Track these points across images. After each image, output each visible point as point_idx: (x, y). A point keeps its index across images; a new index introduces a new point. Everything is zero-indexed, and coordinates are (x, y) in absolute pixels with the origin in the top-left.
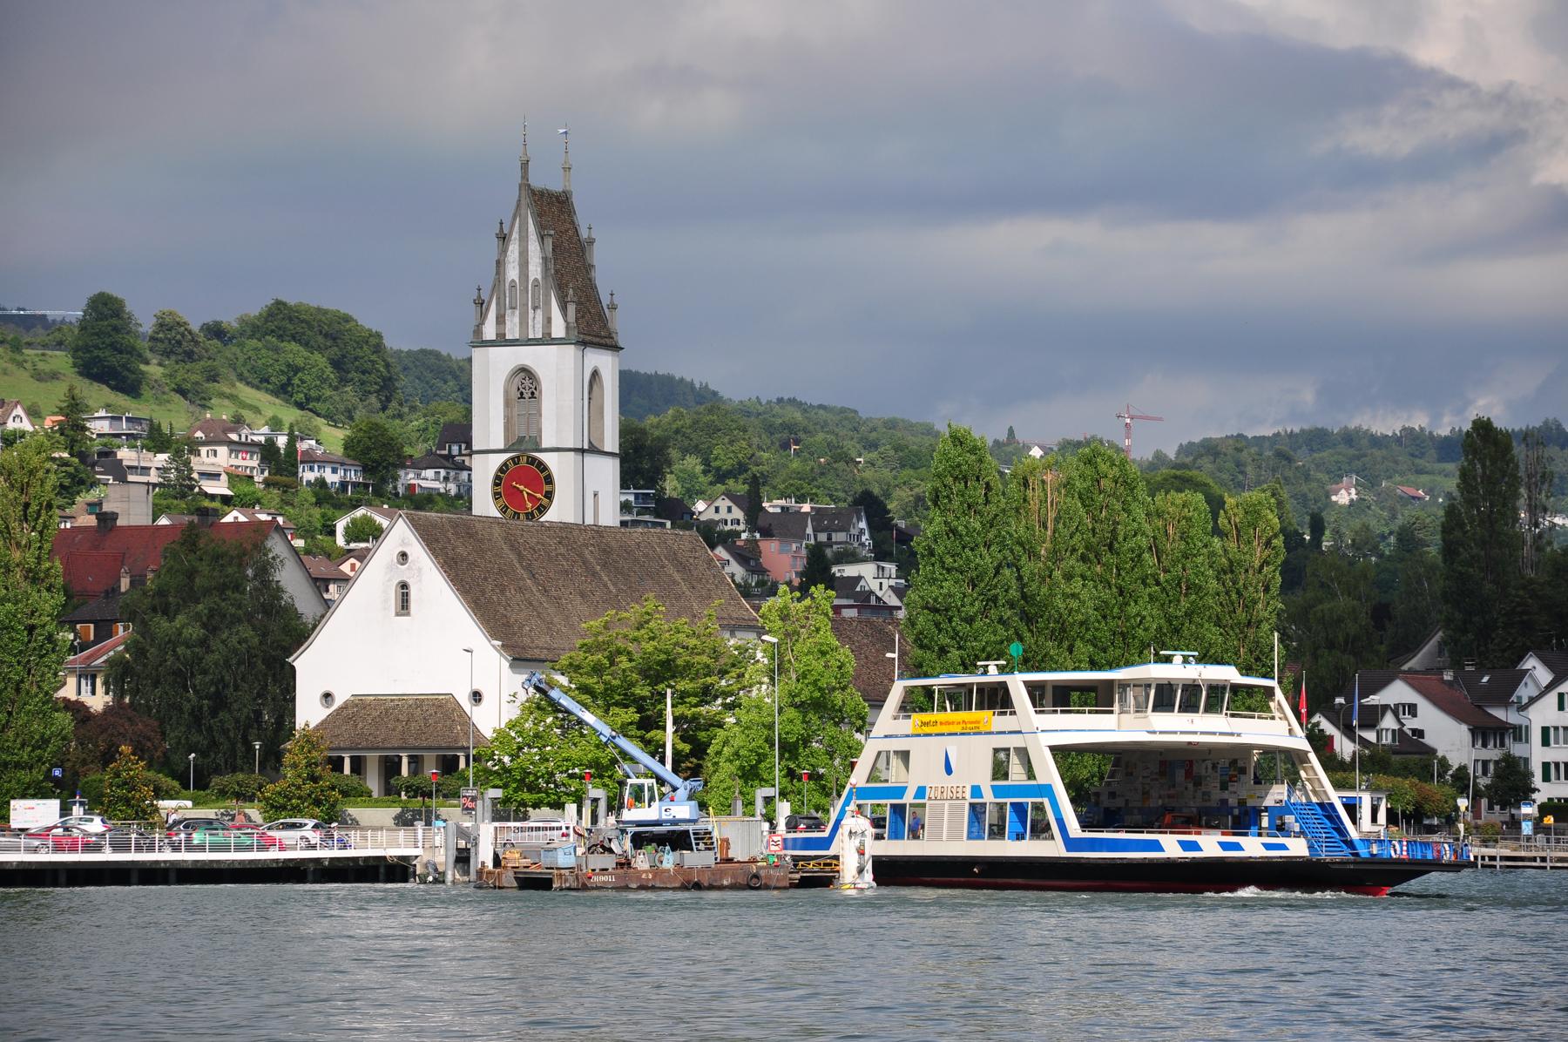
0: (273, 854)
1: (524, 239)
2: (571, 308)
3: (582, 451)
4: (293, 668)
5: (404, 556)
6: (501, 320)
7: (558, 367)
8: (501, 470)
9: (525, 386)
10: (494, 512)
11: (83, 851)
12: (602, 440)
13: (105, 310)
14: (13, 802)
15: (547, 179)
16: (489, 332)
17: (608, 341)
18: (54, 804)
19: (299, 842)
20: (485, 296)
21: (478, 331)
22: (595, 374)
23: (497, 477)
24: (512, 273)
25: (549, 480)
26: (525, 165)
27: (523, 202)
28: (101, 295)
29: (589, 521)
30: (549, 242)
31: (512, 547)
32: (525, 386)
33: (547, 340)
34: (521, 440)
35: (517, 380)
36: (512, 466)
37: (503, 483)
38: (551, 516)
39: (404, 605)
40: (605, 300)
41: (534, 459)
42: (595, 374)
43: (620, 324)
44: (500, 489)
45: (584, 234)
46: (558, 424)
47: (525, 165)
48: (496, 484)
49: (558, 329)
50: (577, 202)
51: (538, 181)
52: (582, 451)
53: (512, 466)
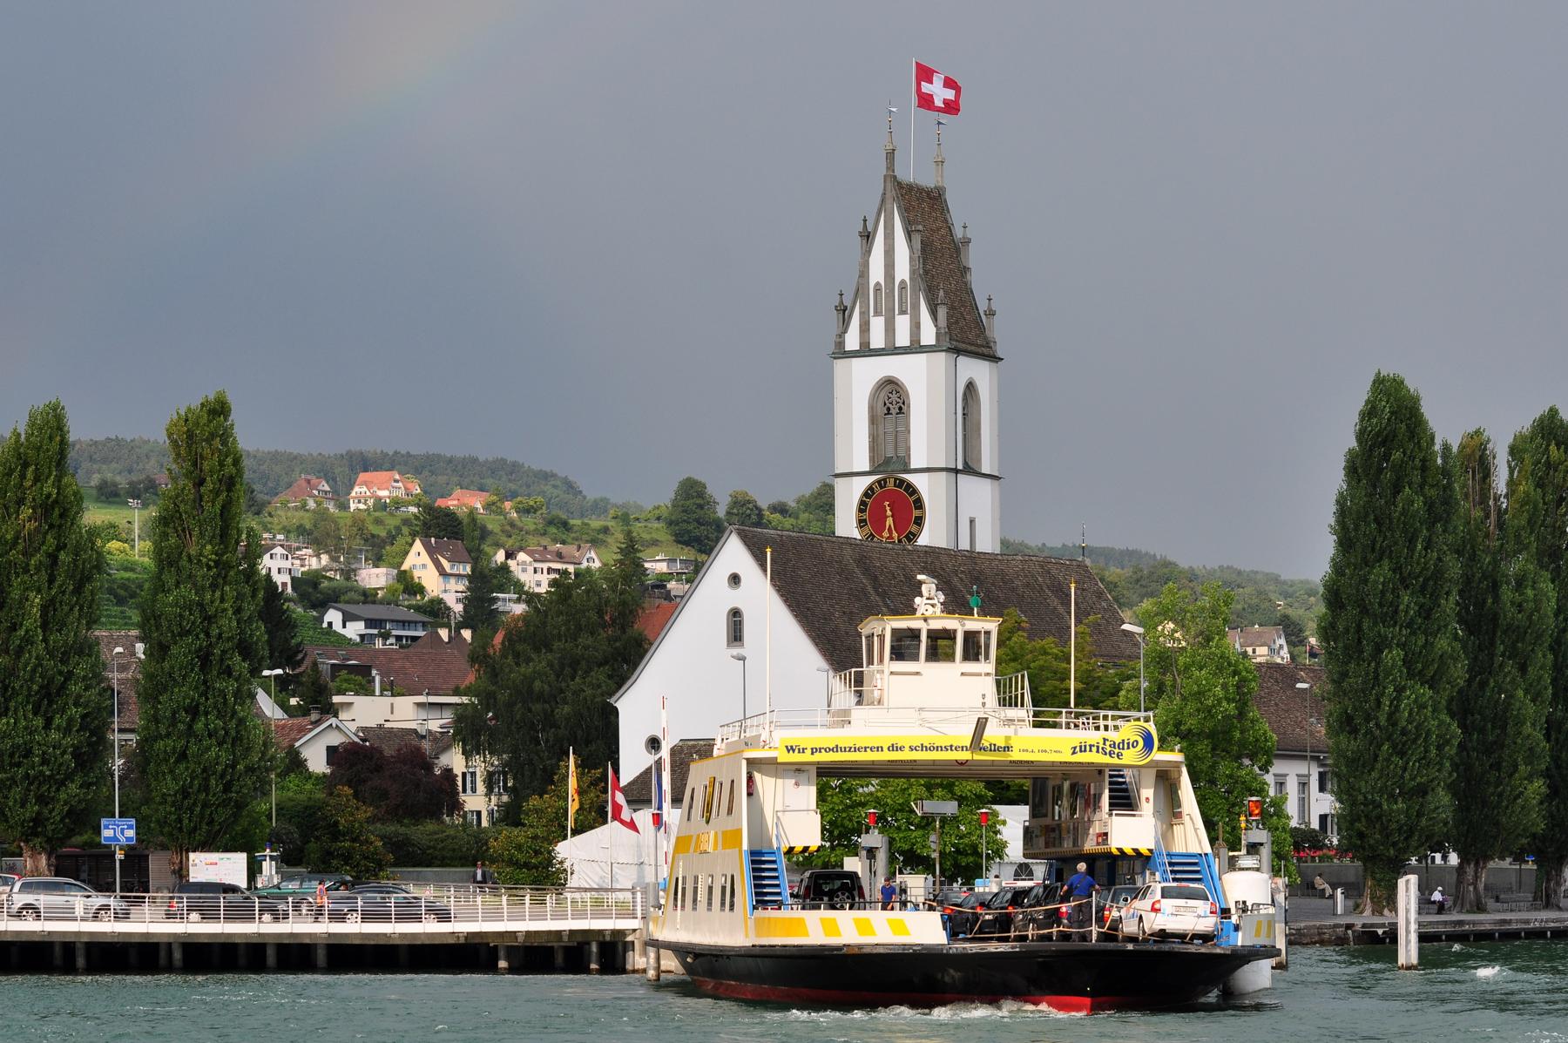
0: (429, 927)
1: (889, 236)
2: (942, 312)
3: (956, 471)
4: (615, 712)
5: (735, 579)
6: (865, 328)
7: (925, 379)
8: (866, 494)
9: (891, 402)
10: (856, 534)
11: (228, 919)
12: (979, 460)
13: (692, 492)
14: (244, 855)
15: (913, 172)
16: (852, 341)
17: (985, 351)
18: (240, 859)
19: (79, 914)
20: (848, 303)
21: (840, 344)
22: (970, 387)
23: (862, 503)
24: (876, 274)
25: (919, 504)
26: (891, 155)
27: (888, 195)
28: (688, 479)
29: (964, 545)
30: (917, 239)
31: (867, 571)
32: (891, 402)
33: (915, 348)
34: (888, 461)
35: (883, 394)
36: (878, 490)
37: (869, 506)
38: (923, 540)
39: (736, 633)
40: (982, 307)
41: (902, 481)
42: (970, 387)
43: (1000, 332)
44: (866, 516)
45: (959, 233)
46: (927, 442)
47: (891, 155)
48: (860, 511)
49: (928, 335)
50: (950, 198)
51: (900, 174)
52: (956, 471)
53: (878, 490)
